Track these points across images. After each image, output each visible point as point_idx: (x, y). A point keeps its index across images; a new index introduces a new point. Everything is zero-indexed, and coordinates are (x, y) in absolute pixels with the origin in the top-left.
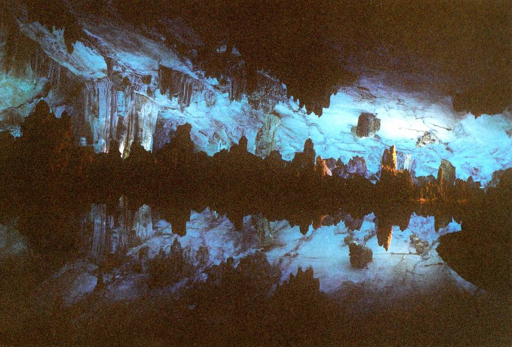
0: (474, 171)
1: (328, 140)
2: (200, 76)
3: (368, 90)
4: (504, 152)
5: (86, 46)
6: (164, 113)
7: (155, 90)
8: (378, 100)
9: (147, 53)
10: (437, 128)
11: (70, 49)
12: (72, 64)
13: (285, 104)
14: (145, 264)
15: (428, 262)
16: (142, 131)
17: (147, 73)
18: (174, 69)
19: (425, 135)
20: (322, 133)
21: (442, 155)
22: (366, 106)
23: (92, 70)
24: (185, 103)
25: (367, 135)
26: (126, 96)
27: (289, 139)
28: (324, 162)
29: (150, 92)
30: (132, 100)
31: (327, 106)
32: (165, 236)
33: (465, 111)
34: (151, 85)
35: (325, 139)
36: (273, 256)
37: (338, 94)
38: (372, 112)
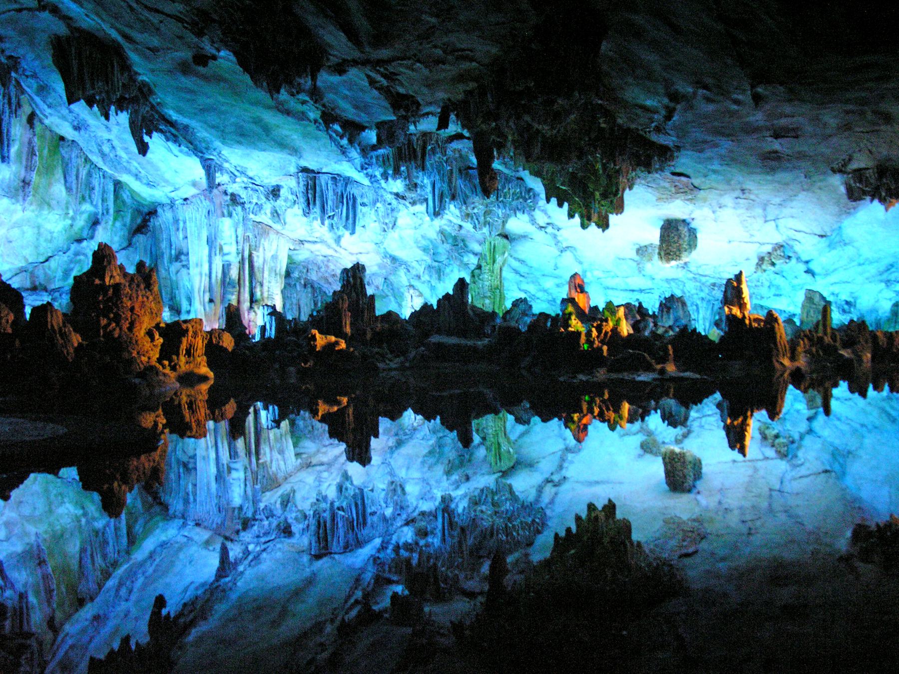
0: (846, 307)
2: (371, 177)
3: (688, 177)
5: (168, 140)
6: (295, 252)
9: (282, 145)
10: (798, 236)
11: (143, 149)
14: (296, 519)
15: (803, 471)
16: (262, 285)
17: (273, 181)
19: (775, 249)
20: (581, 263)
22: (678, 209)
23: (173, 185)
24: (346, 227)
28: (622, 309)
32: (318, 468)
34: (280, 202)
36: (523, 484)
37: (635, 187)
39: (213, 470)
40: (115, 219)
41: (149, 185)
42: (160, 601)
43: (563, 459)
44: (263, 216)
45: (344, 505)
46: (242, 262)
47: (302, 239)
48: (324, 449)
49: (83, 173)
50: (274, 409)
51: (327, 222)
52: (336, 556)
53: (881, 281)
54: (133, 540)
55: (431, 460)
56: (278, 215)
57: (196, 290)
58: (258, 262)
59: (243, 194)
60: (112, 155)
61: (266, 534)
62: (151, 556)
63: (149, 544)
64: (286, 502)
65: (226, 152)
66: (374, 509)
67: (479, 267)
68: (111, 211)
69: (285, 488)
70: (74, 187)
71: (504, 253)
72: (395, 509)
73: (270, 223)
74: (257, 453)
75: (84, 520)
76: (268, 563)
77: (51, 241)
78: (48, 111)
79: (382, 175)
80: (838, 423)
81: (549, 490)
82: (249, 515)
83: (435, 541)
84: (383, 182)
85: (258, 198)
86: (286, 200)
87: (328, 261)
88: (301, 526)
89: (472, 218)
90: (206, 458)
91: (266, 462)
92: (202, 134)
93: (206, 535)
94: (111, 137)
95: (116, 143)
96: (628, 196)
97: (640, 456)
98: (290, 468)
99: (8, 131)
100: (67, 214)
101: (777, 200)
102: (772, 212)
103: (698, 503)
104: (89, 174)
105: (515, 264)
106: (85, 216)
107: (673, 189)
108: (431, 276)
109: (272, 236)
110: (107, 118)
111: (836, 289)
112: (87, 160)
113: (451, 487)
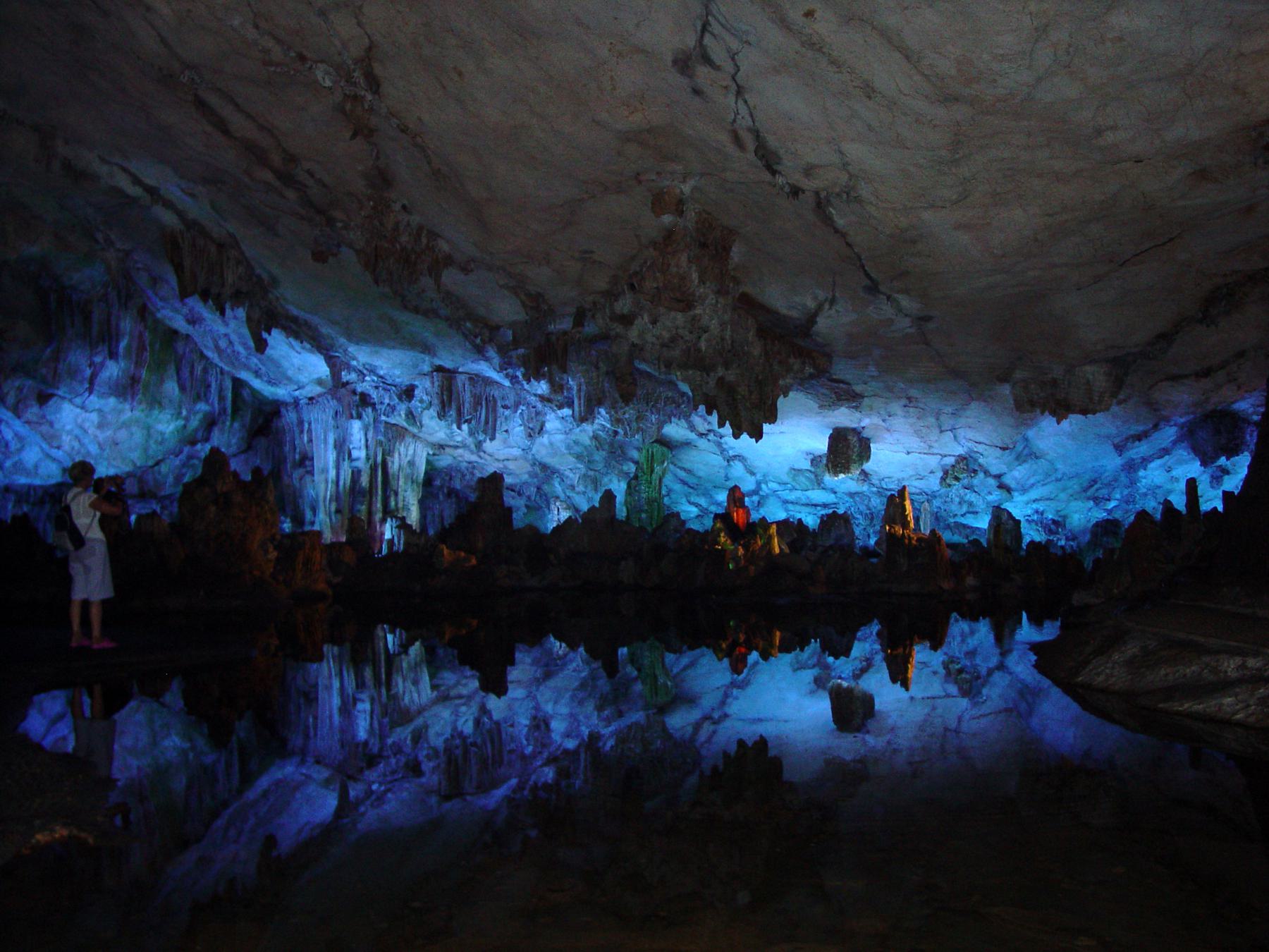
1: (763, 486)
2: (513, 379)
4: (1108, 485)
8: (866, 401)
10: (980, 448)
11: (261, 346)
13: (683, 423)
15: (985, 709)
16: (396, 494)
20: (753, 474)
21: (990, 498)
22: (844, 417)
23: (297, 383)
24: (485, 432)
25: (846, 469)
28: (774, 526)
32: (457, 702)
33: (1038, 411)
34: (415, 403)
35: (759, 484)
36: (679, 721)
37: (791, 394)
38: (854, 425)
39: (336, 701)
40: (233, 420)
41: (269, 382)
42: (271, 841)
43: (726, 696)
45: (479, 741)
46: (373, 469)
47: (442, 443)
48: (464, 681)
49: (199, 369)
50: (401, 634)
51: (465, 427)
52: (468, 798)
53: (1089, 499)
54: (247, 779)
55: (580, 695)
56: (414, 417)
57: (321, 498)
58: (394, 466)
59: (374, 394)
61: (394, 772)
62: (265, 794)
63: (264, 782)
64: (418, 736)
65: (352, 349)
66: (513, 746)
67: (636, 477)
68: (229, 411)
69: (419, 721)
70: (188, 385)
72: (535, 746)
73: (405, 424)
75: (191, 755)
76: (393, 803)
77: (161, 443)
78: (160, 304)
79: (524, 375)
81: (707, 728)
82: (375, 750)
85: (390, 398)
86: (421, 401)
88: (431, 764)
90: (329, 688)
91: (397, 693)
93: (325, 773)
94: (228, 331)
95: (234, 337)
97: (812, 692)
98: (424, 700)
99: (118, 325)
100: (180, 413)
101: (949, 410)
103: (864, 742)
104: (205, 370)
105: (682, 474)
106: (200, 416)
109: (409, 439)
110: (223, 313)
112: (202, 354)
113: (602, 724)
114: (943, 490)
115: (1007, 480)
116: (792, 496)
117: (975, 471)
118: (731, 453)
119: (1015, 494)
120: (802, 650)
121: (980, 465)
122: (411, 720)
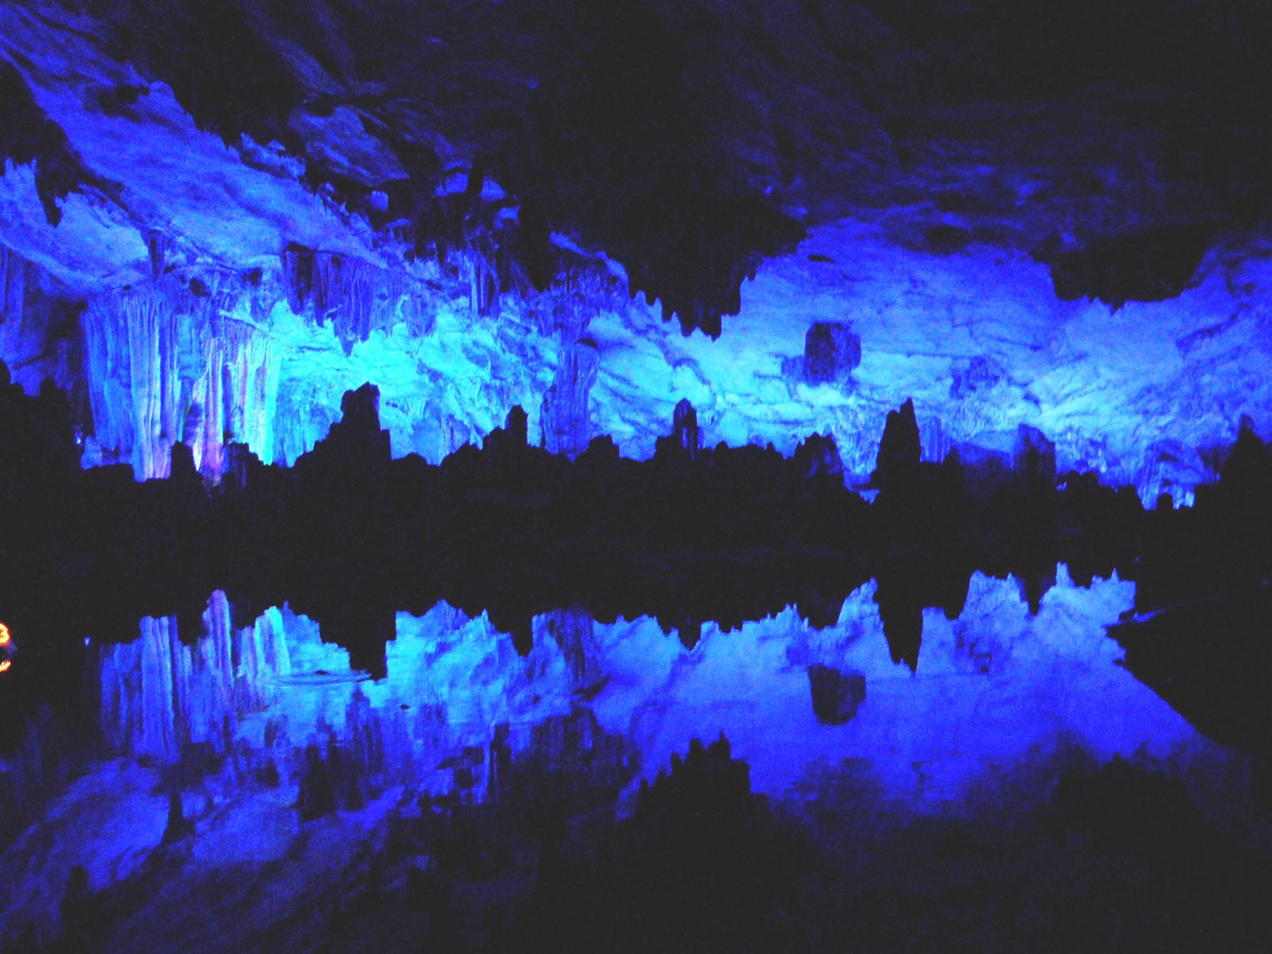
0: (1091, 449)
1: (719, 399)
2: (392, 259)
7: (273, 304)
10: (1005, 347)
11: (55, 216)
12: (53, 252)
18: (321, 248)
20: (705, 382)
22: (828, 307)
23: (105, 267)
24: (354, 330)
26: (199, 326)
27: (620, 403)
29: (259, 311)
30: (215, 332)
31: (734, 309)
34: (262, 292)
36: (615, 709)
37: (758, 277)
38: (840, 318)
41: (73, 264)
44: (241, 312)
53: (1137, 412)
60: (16, 225)
71: (589, 368)
73: (252, 321)
74: (236, 661)
80: (1068, 622)
83: (480, 791)
84: (406, 264)
87: (343, 376)
89: (537, 319)
92: (141, 193)
96: (746, 289)
102: (961, 313)
105: (613, 383)
107: (814, 280)
108: (490, 401)
111: (1075, 422)
114: (953, 403)
115: (1036, 388)
116: (756, 411)
117: (996, 378)
118: (678, 356)
119: (1044, 407)
120: (774, 616)
121: (1003, 371)
122: (266, 708)
